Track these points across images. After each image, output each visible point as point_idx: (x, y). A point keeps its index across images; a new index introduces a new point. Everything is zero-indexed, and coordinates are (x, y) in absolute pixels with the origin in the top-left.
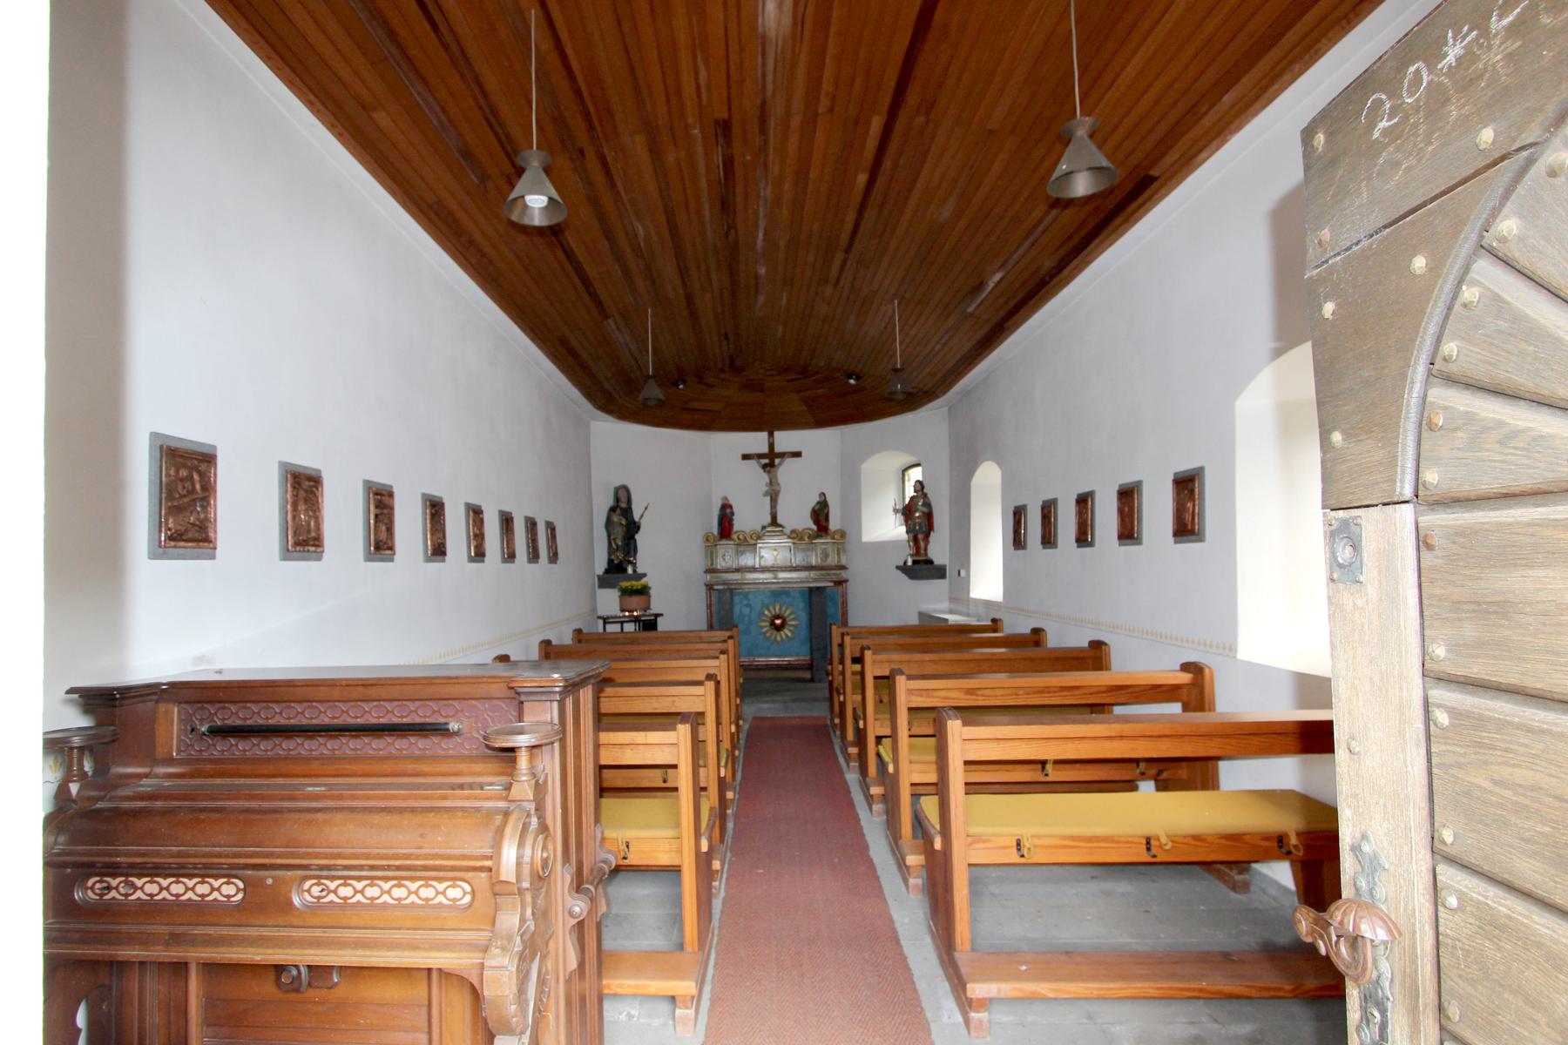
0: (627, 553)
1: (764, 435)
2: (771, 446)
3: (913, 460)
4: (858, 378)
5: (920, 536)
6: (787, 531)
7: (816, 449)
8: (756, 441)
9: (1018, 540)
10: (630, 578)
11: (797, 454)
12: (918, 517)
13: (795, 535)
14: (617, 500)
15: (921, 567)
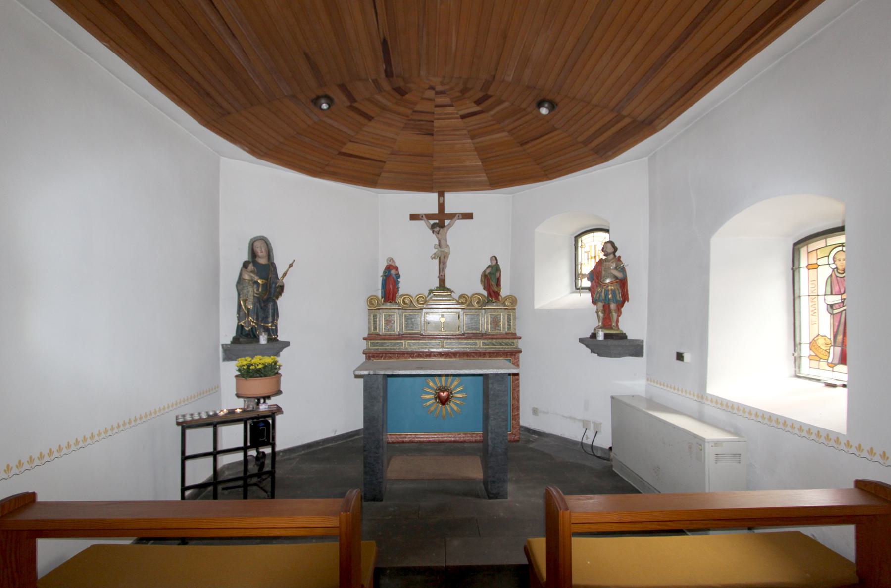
1: (434, 197)
2: (441, 206)
4: (553, 106)
5: (613, 306)
6: (456, 296)
7: (489, 218)
8: (427, 202)
10: (264, 352)
11: (469, 216)
13: (465, 301)
14: (253, 254)
15: (611, 342)
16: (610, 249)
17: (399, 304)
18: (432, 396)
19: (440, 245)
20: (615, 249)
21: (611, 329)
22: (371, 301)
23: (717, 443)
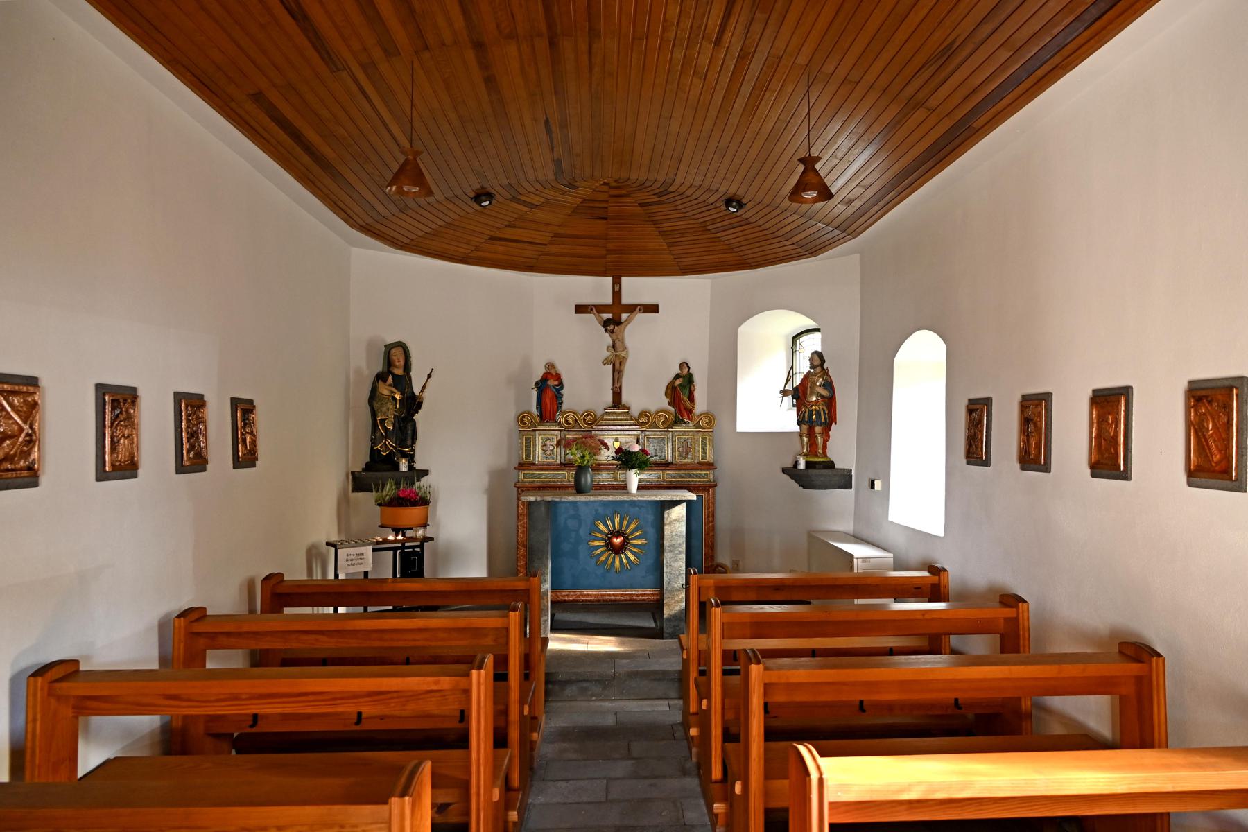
0: (402, 443)
2: (617, 295)
3: (811, 324)
5: (818, 429)
7: (677, 310)
8: (597, 288)
9: (975, 448)
11: (653, 309)
12: (814, 398)
14: (389, 362)
16: (817, 362)
17: (559, 424)
18: (602, 543)
19: (614, 347)
20: (823, 361)
21: (816, 455)
22: (521, 418)
23: (864, 560)
